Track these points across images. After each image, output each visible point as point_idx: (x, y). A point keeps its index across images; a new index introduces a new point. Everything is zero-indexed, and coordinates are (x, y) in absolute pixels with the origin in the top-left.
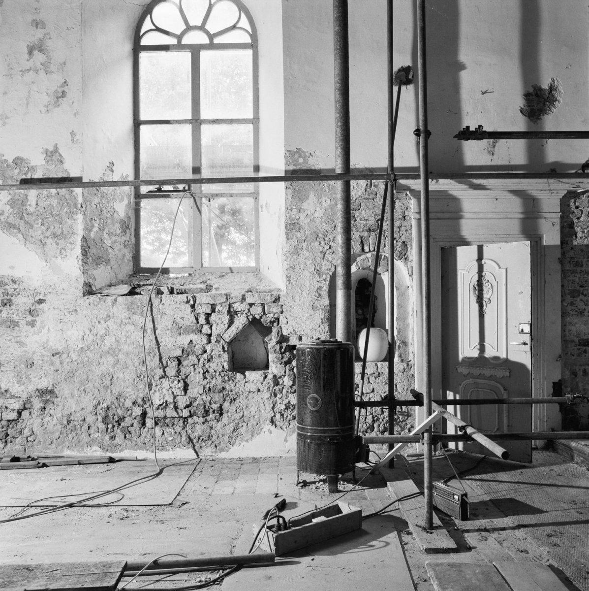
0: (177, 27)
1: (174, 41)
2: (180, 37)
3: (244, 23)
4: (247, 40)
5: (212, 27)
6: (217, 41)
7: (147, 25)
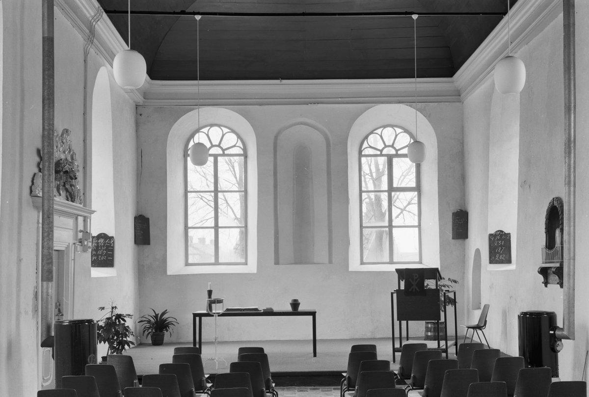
0: (380, 146)
1: (379, 153)
2: (381, 151)
3: (240, 144)
4: (242, 152)
5: (224, 145)
6: (226, 152)
7: (365, 145)
